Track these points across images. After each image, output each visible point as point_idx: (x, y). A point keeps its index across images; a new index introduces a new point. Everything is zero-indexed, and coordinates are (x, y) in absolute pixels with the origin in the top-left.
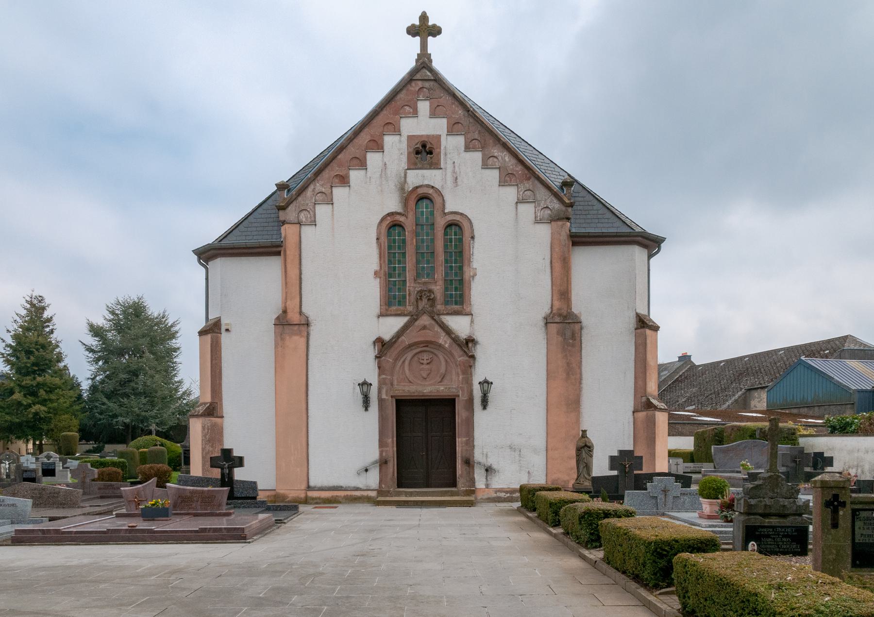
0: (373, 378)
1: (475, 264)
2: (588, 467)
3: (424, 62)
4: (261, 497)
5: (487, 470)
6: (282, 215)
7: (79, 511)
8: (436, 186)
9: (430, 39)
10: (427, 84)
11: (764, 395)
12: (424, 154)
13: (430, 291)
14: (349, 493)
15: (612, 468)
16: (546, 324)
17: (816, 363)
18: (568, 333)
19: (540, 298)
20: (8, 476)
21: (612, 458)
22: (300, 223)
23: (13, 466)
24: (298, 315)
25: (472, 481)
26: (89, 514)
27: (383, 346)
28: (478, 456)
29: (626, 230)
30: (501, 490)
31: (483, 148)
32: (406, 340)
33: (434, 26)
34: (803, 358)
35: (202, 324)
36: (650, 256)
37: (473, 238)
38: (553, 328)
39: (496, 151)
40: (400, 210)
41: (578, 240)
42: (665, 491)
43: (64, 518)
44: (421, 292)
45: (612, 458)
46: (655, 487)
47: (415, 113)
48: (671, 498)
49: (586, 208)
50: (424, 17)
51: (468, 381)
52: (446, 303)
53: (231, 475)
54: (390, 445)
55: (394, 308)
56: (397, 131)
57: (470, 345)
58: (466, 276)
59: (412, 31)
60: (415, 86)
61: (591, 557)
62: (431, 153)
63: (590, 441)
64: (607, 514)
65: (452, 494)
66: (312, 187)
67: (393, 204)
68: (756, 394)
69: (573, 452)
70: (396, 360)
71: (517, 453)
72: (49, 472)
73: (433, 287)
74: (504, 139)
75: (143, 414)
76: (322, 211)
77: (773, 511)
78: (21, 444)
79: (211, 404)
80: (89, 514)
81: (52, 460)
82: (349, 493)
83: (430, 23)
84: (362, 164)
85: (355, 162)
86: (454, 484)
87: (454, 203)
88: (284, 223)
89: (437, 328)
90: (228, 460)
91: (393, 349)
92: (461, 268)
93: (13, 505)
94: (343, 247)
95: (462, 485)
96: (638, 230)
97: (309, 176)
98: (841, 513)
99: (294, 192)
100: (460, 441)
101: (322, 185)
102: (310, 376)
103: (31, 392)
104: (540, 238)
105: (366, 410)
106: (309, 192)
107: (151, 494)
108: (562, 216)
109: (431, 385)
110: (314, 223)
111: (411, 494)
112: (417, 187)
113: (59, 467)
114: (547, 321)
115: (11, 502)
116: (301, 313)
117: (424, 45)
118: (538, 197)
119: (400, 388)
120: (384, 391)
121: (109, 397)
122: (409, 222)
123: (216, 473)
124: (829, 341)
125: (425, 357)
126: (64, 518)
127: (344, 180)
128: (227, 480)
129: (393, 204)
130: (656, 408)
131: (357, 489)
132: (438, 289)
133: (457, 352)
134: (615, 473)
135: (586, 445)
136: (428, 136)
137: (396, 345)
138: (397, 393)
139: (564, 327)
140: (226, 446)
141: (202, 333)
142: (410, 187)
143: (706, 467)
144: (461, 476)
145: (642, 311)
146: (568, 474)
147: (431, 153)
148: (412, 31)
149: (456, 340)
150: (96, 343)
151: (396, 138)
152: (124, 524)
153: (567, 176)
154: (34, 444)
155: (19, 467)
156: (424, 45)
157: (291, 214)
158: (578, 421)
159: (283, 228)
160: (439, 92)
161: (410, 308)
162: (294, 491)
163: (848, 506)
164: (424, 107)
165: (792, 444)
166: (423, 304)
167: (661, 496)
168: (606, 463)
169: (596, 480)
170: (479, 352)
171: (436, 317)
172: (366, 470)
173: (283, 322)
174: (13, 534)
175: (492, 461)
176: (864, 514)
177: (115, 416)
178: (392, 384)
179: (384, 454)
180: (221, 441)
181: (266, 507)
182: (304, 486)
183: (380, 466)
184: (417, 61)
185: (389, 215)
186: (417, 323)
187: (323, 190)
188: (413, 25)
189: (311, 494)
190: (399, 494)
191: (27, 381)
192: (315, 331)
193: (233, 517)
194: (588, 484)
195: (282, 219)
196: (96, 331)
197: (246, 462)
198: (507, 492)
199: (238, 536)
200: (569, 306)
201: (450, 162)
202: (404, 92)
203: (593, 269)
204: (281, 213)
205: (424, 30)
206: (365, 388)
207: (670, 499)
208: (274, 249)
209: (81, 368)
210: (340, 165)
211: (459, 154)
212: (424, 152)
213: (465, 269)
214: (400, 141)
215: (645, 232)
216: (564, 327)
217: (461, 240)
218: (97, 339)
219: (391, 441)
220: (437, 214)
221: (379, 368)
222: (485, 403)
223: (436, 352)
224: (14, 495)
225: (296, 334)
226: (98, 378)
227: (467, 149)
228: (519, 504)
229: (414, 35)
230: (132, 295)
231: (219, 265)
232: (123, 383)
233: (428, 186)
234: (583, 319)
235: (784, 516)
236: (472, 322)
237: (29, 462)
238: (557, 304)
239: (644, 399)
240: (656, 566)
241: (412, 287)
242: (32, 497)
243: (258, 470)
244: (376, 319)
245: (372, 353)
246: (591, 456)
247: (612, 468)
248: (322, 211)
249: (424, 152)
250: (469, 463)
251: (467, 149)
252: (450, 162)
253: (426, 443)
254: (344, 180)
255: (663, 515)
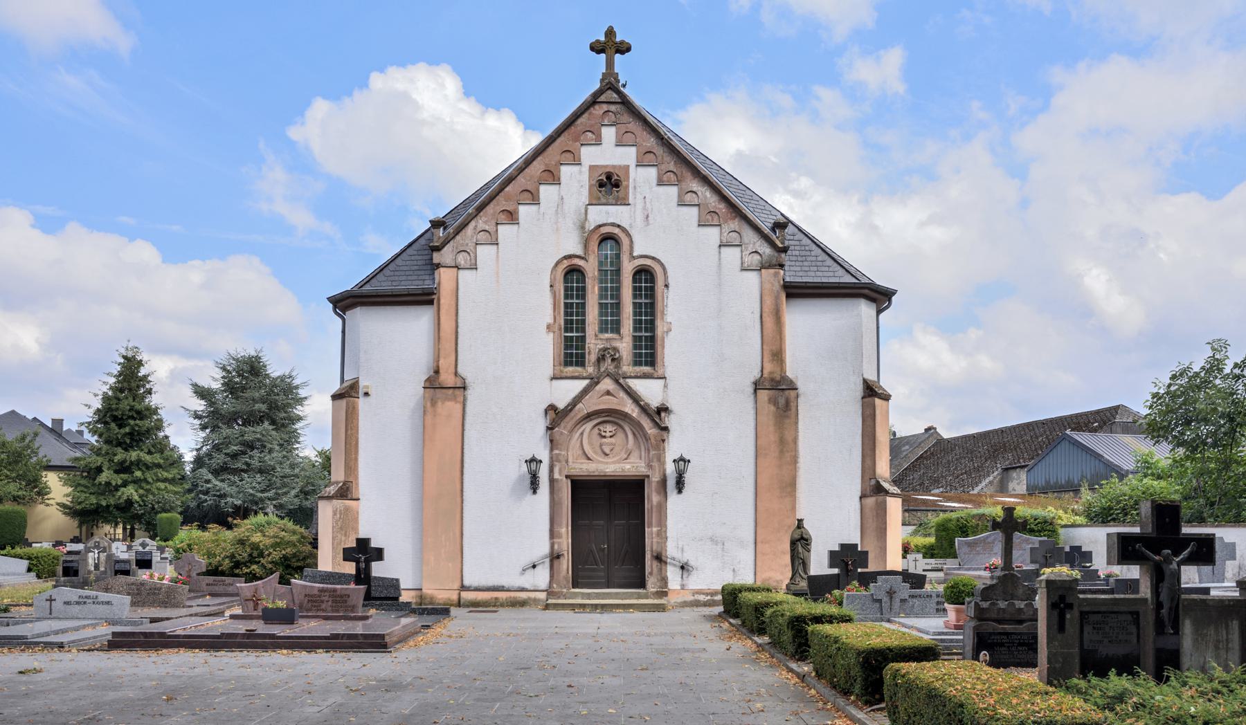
0: (544, 455)
1: (669, 318)
2: (805, 565)
3: (610, 83)
4: (405, 597)
5: (682, 568)
6: (437, 257)
7: (184, 611)
8: (623, 224)
9: (617, 56)
10: (613, 108)
11: (1023, 475)
12: (609, 186)
13: (616, 350)
14: (512, 594)
15: (832, 566)
16: (755, 390)
17: (1083, 438)
18: (782, 401)
19: (749, 361)
20: (97, 567)
21: (832, 554)
22: (457, 267)
23: (103, 556)
24: (452, 376)
25: (664, 580)
26: (196, 615)
27: (556, 416)
28: (671, 550)
29: (848, 279)
30: (699, 592)
31: (679, 182)
32: (583, 408)
33: (622, 42)
34: (1068, 432)
35: (336, 387)
36: (879, 312)
37: (667, 286)
38: (764, 395)
39: (695, 185)
40: (580, 252)
41: (795, 291)
42: (891, 593)
43: (168, 619)
44: (605, 349)
45: (832, 554)
46: (880, 588)
47: (598, 141)
48: (898, 600)
49: (803, 253)
50: (610, 33)
51: (661, 462)
52: (637, 363)
53: (368, 569)
54: (564, 536)
55: (571, 369)
56: (577, 162)
57: (663, 414)
58: (660, 330)
59: (597, 48)
60: (598, 110)
61: (799, 670)
62: (617, 186)
63: (807, 533)
64: (818, 619)
65: (639, 597)
66: (473, 224)
67: (573, 246)
68: (1014, 475)
69: (787, 546)
70: (571, 431)
71: (720, 546)
72: (145, 563)
73: (617, 344)
74: (705, 171)
75: (259, 495)
76: (485, 253)
77: (1007, 616)
78: (107, 528)
79: (344, 483)
80: (196, 615)
81: (147, 549)
82: (512, 594)
83: (618, 39)
84: (534, 199)
85: (526, 195)
86: (642, 584)
87: (643, 245)
88: (438, 266)
89: (622, 394)
90: (364, 553)
91: (568, 419)
92: (652, 322)
93: (108, 603)
94: (507, 297)
95: (652, 584)
96: (864, 280)
97: (470, 211)
98: (1068, 616)
99: (451, 230)
100: (651, 532)
101: (485, 222)
102: (466, 451)
103: (123, 468)
104: (748, 290)
105: (535, 492)
106: (470, 229)
107: (271, 593)
108: (774, 262)
109: (614, 463)
110: (474, 267)
111: (589, 596)
112: (600, 226)
113: (156, 557)
114: (757, 386)
115: (107, 600)
116: (456, 374)
117: (610, 64)
118: (746, 239)
119: (577, 466)
120: (556, 470)
121: (216, 473)
122: (591, 268)
123: (350, 568)
124: (1098, 412)
125: (609, 428)
126: (168, 619)
127: (512, 217)
128: (363, 576)
129: (573, 246)
130: (887, 492)
131: (523, 590)
132: (625, 346)
133: (646, 423)
134: (836, 571)
135: (802, 538)
136: (614, 167)
137: (572, 414)
138: (573, 472)
139: (777, 391)
140: (361, 536)
141: (336, 397)
142: (591, 225)
143: (950, 563)
144: (651, 573)
145: (871, 376)
146: (779, 573)
147: (617, 186)
148: (597, 48)
149: (644, 409)
150: (202, 408)
151: (575, 169)
152: (241, 627)
153: (779, 216)
154: (124, 529)
155: (110, 557)
156: (610, 64)
157: (445, 256)
158: (794, 508)
159: (436, 272)
160: (626, 118)
161: (590, 369)
162: (442, 593)
163: (1075, 608)
164: (609, 134)
165: (1049, 536)
166: (608, 365)
167: (885, 599)
168: (825, 560)
169: (813, 581)
170: (670, 421)
171: (621, 381)
172: (534, 567)
173: (433, 384)
174: (110, 637)
175: (688, 557)
176: (1093, 618)
177: (223, 496)
178: (567, 462)
179: (556, 547)
180: (356, 530)
181: (407, 609)
182: (457, 585)
183: (551, 561)
184: (602, 81)
185: (566, 258)
186: (598, 388)
187: (487, 228)
188: (598, 41)
189: (467, 596)
190: (575, 595)
191: (120, 455)
192: (473, 396)
193: (370, 621)
194: (803, 584)
195: (435, 261)
196: (201, 393)
197: (386, 554)
198: (707, 594)
199: (377, 643)
200: (783, 369)
201: (640, 197)
202: (586, 115)
203: (807, 324)
204: (435, 255)
205: (610, 46)
206: (533, 466)
207: (897, 604)
208: (425, 298)
209: (185, 439)
210: (508, 199)
211: (651, 188)
212: (609, 185)
213: (659, 323)
214: (580, 172)
215: (873, 284)
216: (777, 391)
217: (652, 289)
218: (203, 402)
219: (565, 531)
220: (625, 258)
221: (551, 441)
222: (680, 485)
223: (621, 423)
224: (107, 590)
225: (449, 400)
226: (204, 449)
227: (661, 183)
228: (721, 609)
229: (599, 52)
230: (246, 349)
231: (359, 316)
232: (234, 456)
233: (613, 225)
234: (799, 384)
235: (1020, 622)
236: (665, 386)
237: (120, 550)
238: (769, 367)
239: (873, 482)
240: (870, 676)
241: (594, 344)
242: (129, 594)
243: (398, 566)
244: (548, 381)
245: (541, 424)
246: (809, 551)
247: (832, 566)
248: (485, 253)
249: (609, 185)
250: (659, 558)
251: (661, 183)
252: (640, 197)
253: (610, 527)
254: (512, 217)
255: (889, 621)
